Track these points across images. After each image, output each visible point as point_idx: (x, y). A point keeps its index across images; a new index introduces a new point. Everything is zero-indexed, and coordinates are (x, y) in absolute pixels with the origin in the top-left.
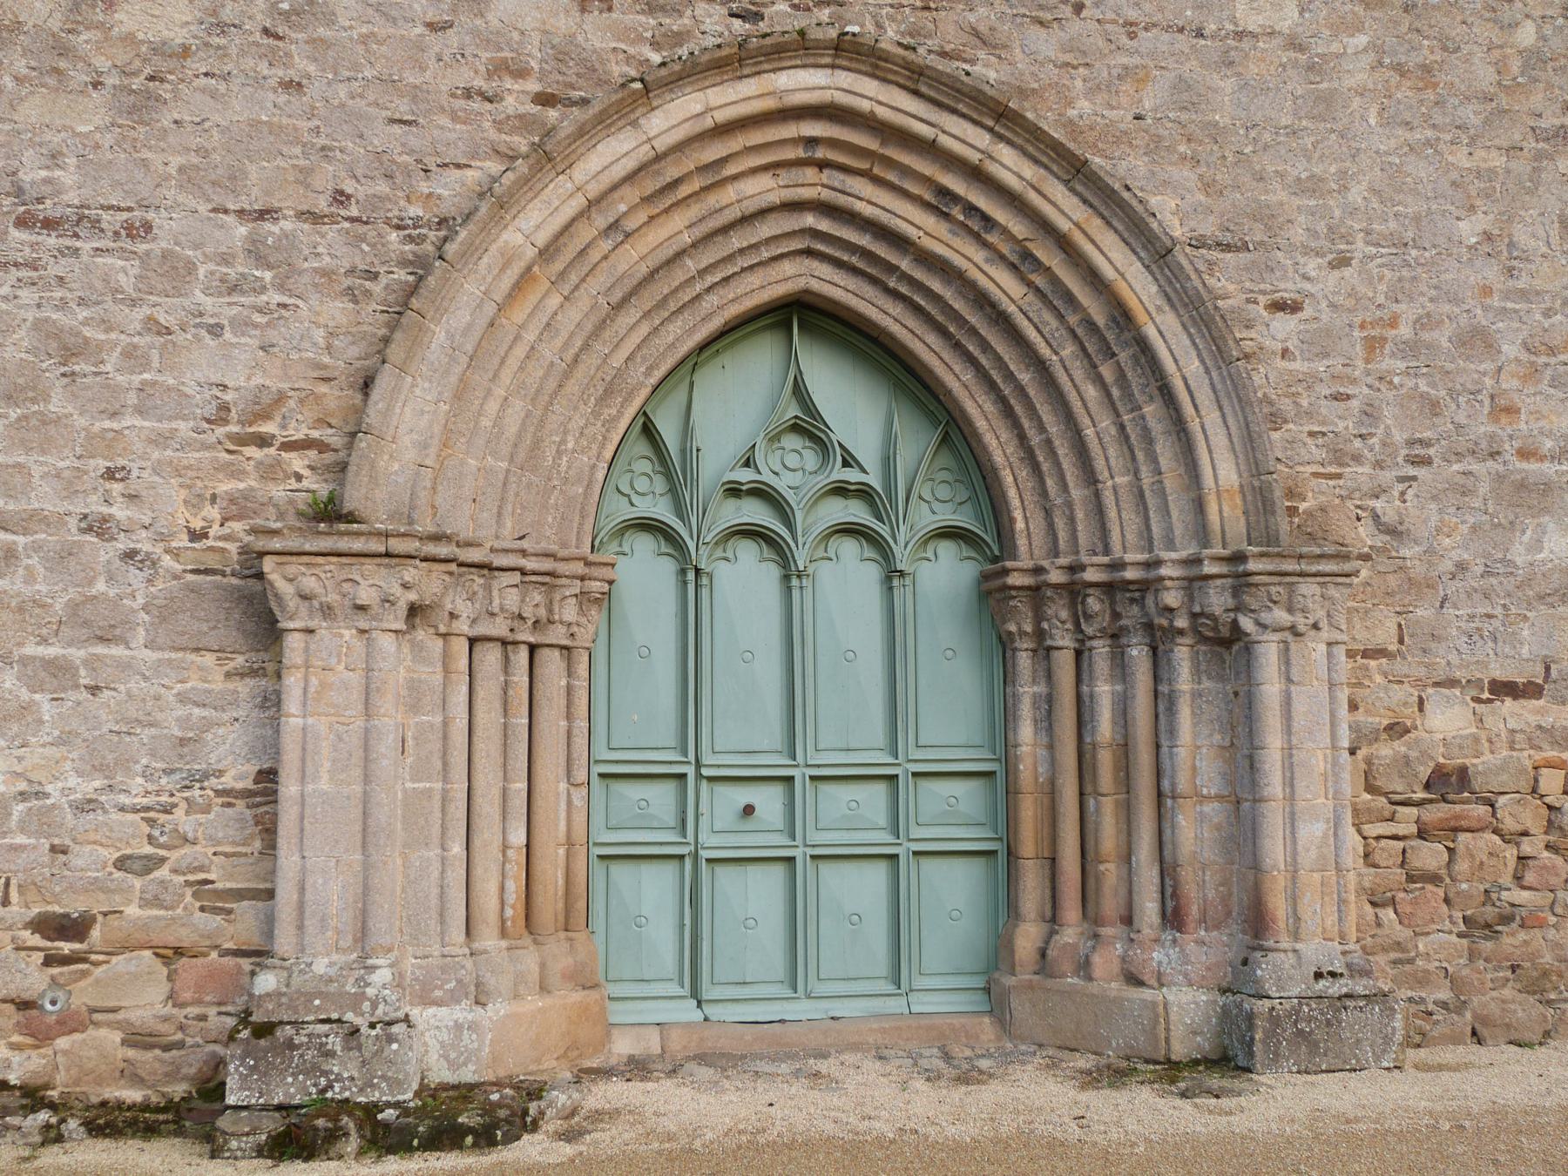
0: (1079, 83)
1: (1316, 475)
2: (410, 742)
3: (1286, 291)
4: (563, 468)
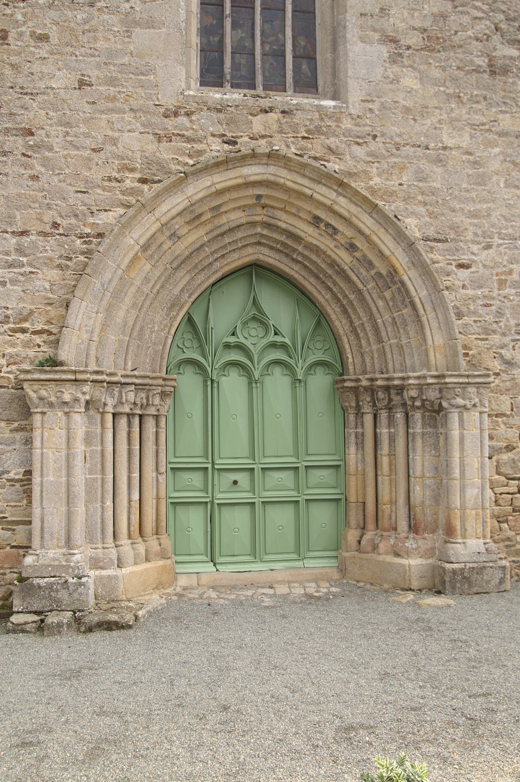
0: (375, 170)
1: (476, 339)
2: (88, 458)
3: (464, 259)
4: (153, 338)
